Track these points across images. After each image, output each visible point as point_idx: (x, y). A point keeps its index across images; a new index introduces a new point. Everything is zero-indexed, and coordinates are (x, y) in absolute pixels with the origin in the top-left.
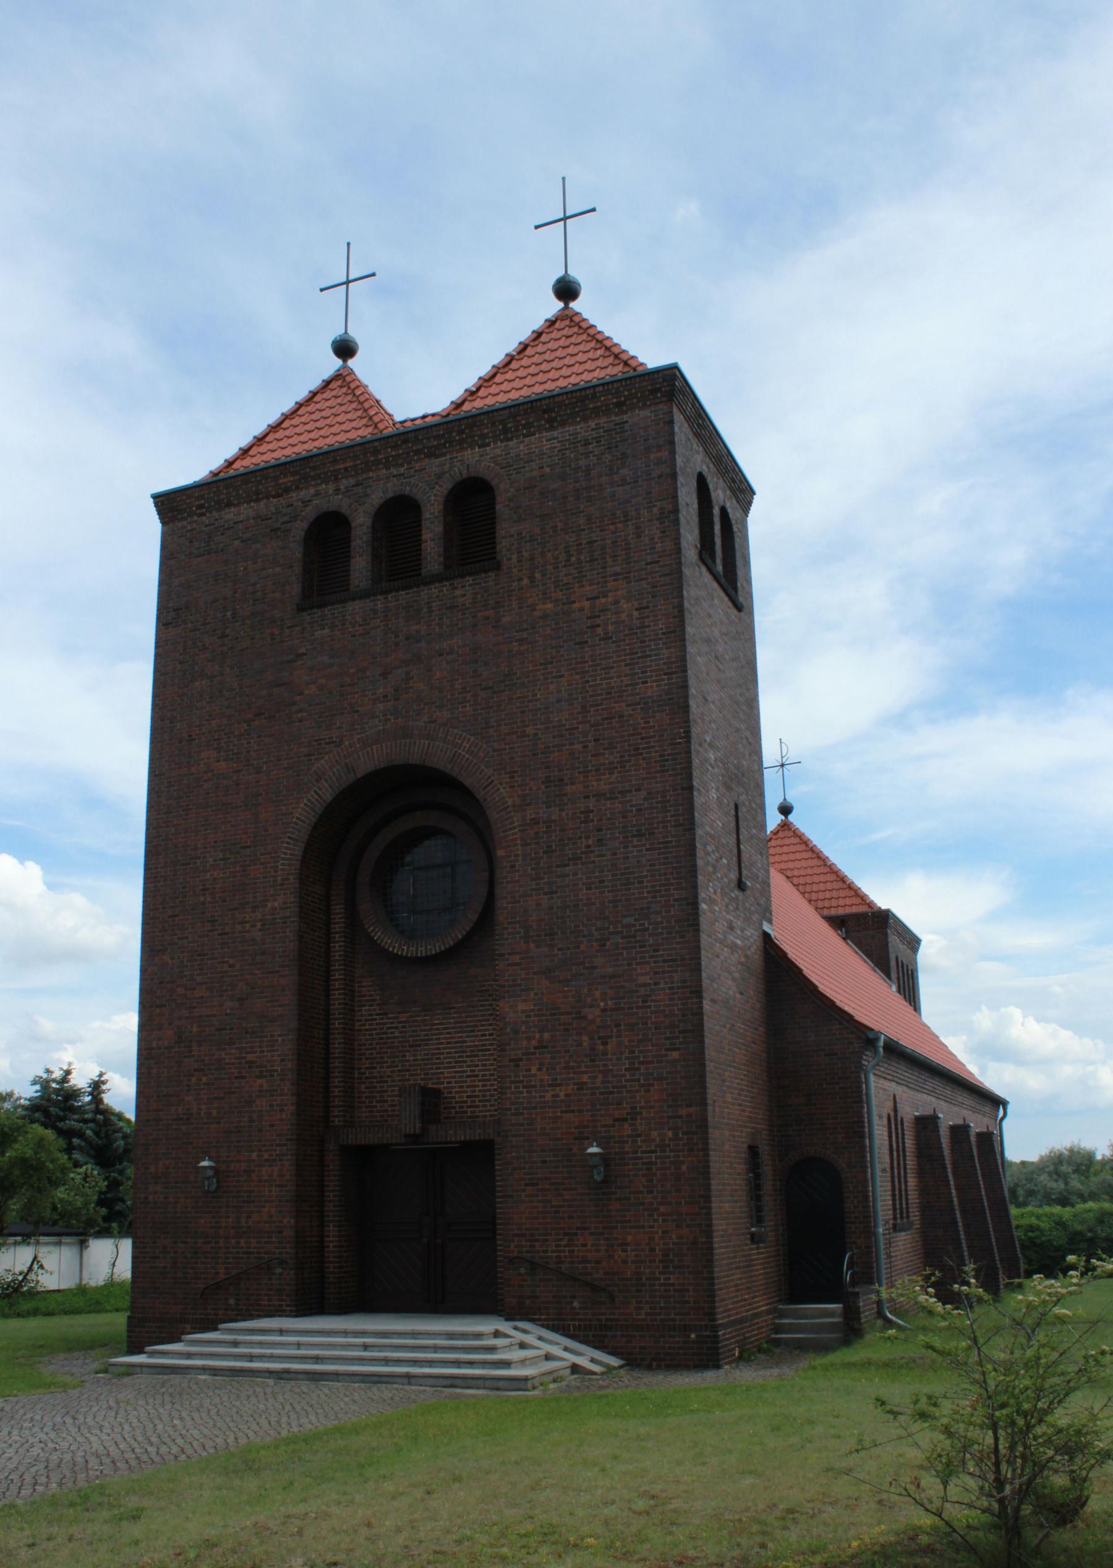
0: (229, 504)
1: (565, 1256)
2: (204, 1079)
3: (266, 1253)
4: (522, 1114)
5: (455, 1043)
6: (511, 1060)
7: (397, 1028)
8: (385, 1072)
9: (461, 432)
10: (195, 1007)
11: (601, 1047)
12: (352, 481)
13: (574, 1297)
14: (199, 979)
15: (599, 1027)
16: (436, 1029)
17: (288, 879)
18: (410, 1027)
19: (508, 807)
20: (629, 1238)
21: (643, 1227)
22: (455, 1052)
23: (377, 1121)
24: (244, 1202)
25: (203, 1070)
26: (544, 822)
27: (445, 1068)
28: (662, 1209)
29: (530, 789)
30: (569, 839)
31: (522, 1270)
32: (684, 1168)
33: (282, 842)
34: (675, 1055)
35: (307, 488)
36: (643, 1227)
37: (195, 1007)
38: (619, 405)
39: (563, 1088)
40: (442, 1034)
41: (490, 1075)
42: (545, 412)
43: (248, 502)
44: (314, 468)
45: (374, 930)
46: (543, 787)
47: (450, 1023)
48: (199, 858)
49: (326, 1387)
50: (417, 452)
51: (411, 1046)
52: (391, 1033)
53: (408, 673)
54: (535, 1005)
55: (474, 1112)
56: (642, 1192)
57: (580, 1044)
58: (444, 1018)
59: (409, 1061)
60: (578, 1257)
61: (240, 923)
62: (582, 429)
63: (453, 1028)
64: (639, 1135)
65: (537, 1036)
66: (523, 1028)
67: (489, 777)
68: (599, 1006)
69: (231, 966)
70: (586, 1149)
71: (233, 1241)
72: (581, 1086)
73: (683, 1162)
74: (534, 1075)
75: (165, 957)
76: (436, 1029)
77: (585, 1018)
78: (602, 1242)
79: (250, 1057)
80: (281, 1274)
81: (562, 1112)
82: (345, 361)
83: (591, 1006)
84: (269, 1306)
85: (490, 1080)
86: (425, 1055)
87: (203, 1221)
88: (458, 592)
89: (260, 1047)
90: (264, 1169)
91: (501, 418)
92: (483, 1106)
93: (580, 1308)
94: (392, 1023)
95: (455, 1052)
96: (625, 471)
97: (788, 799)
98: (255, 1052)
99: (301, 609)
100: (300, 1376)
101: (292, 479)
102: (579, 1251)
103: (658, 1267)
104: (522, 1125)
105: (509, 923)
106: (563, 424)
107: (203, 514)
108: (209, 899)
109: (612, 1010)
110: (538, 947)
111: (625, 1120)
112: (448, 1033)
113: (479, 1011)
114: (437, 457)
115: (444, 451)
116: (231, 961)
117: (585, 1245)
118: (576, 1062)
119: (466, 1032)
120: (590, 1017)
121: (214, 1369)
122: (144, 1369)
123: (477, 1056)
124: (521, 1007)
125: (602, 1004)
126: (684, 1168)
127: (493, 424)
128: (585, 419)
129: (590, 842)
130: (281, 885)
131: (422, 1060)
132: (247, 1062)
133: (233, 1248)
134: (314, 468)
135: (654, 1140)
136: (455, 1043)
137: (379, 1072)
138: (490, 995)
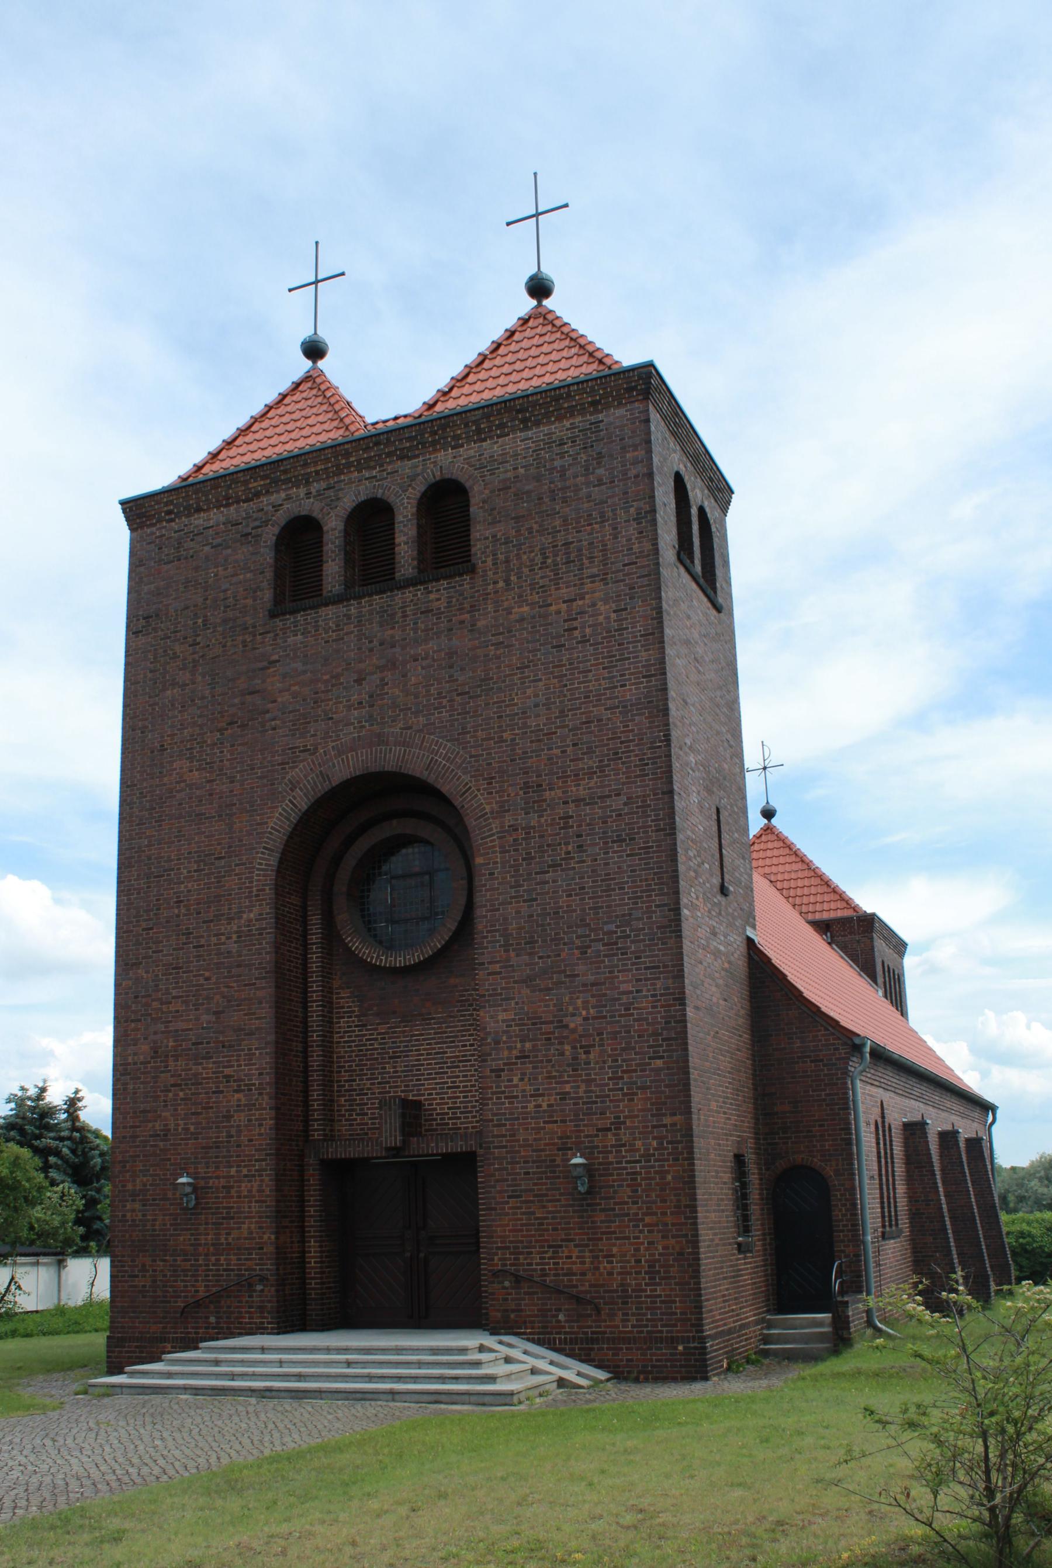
0: (199, 510)
1: (550, 1269)
2: (181, 1094)
3: (246, 1270)
4: (505, 1125)
7: (376, 1039)
8: (364, 1084)
9: (436, 433)
10: (170, 1022)
11: (584, 1056)
14: (174, 993)
17: (264, 890)
20: (615, 1250)
21: (628, 1238)
23: (358, 1135)
24: (223, 1218)
25: (180, 1085)
27: (425, 1079)
28: (648, 1219)
29: (508, 795)
30: (548, 845)
31: (507, 1284)
32: (669, 1177)
33: (257, 853)
34: (659, 1063)
35: (278, 492)
36: (628, 1238)
37: (170, 1022)
38: (594, 403)
39: (546, 1098)
42: (518, 411)
44: (285, 472)
46: (521, 792)
47: (430, 1034)
49: (308, 1405)
51: (390, 1058)
53: (382, 679)
54: (515, 1015)
56: (627, 1203)
57: (562, 1054)
58: (423, 1029)
60: (563, 1269)
61: (215, 935)
62: (558, 429)
64: (624, 1145)
65: (519, 1045)
66: (504, 1038)
67: (467, 784)
69: (207, 979)
70: (570, 1160)
71: (213, 1258)
73: (668, 1172)
74: (516, 1086)
75: (139, 971)
77: (566, 1026)
78: (587, 1254)
79: (227, 1071)
80: (262, 1291)
81: (544, 1122)
82: (315, 362)
83: (573, 1015)
84: (250, 1323)
85: (471, 1091)
86: (405, 1066)
87: (182, 1238)
88: (432, 596)
89: (238, 1061)
91: (474, 418)
92: (465, 1118)
93: (566, 1321)
95: (436, 1064)
97: (771, 803)
98: (233, 1066)
99: (273, 615)
100: (283, 1394)
102: (563, 1263)
103: (644, 1279)
104: (504, 1136)
105: (488, 932)
106: (537, 424)
107: (172, 520)
108: (183, 911)
109: (595, 1018)
110: (517, 955)
111: (609, 1129)
113: (459, 1021)
114: (409, 458)
115: (417, 452)
116: (207, 974)
117: (570, 1257)
118: (557, 1071)
119: (445, 1043)
120: (572, 1025)
121: (196, 1389)
123: (458, 1067)
124: (502, 1016)
125: (584, 1013)
126: (669, 1177)
127: (466, 425)
128: (560, 419)
129: (570, 848)
131: (403, 1071)
132: (225, 1077)
133: (213, 1265)
134: (285, 472)
135: (638, 1150)
137: (359, 1085)
138: (471, 1005)
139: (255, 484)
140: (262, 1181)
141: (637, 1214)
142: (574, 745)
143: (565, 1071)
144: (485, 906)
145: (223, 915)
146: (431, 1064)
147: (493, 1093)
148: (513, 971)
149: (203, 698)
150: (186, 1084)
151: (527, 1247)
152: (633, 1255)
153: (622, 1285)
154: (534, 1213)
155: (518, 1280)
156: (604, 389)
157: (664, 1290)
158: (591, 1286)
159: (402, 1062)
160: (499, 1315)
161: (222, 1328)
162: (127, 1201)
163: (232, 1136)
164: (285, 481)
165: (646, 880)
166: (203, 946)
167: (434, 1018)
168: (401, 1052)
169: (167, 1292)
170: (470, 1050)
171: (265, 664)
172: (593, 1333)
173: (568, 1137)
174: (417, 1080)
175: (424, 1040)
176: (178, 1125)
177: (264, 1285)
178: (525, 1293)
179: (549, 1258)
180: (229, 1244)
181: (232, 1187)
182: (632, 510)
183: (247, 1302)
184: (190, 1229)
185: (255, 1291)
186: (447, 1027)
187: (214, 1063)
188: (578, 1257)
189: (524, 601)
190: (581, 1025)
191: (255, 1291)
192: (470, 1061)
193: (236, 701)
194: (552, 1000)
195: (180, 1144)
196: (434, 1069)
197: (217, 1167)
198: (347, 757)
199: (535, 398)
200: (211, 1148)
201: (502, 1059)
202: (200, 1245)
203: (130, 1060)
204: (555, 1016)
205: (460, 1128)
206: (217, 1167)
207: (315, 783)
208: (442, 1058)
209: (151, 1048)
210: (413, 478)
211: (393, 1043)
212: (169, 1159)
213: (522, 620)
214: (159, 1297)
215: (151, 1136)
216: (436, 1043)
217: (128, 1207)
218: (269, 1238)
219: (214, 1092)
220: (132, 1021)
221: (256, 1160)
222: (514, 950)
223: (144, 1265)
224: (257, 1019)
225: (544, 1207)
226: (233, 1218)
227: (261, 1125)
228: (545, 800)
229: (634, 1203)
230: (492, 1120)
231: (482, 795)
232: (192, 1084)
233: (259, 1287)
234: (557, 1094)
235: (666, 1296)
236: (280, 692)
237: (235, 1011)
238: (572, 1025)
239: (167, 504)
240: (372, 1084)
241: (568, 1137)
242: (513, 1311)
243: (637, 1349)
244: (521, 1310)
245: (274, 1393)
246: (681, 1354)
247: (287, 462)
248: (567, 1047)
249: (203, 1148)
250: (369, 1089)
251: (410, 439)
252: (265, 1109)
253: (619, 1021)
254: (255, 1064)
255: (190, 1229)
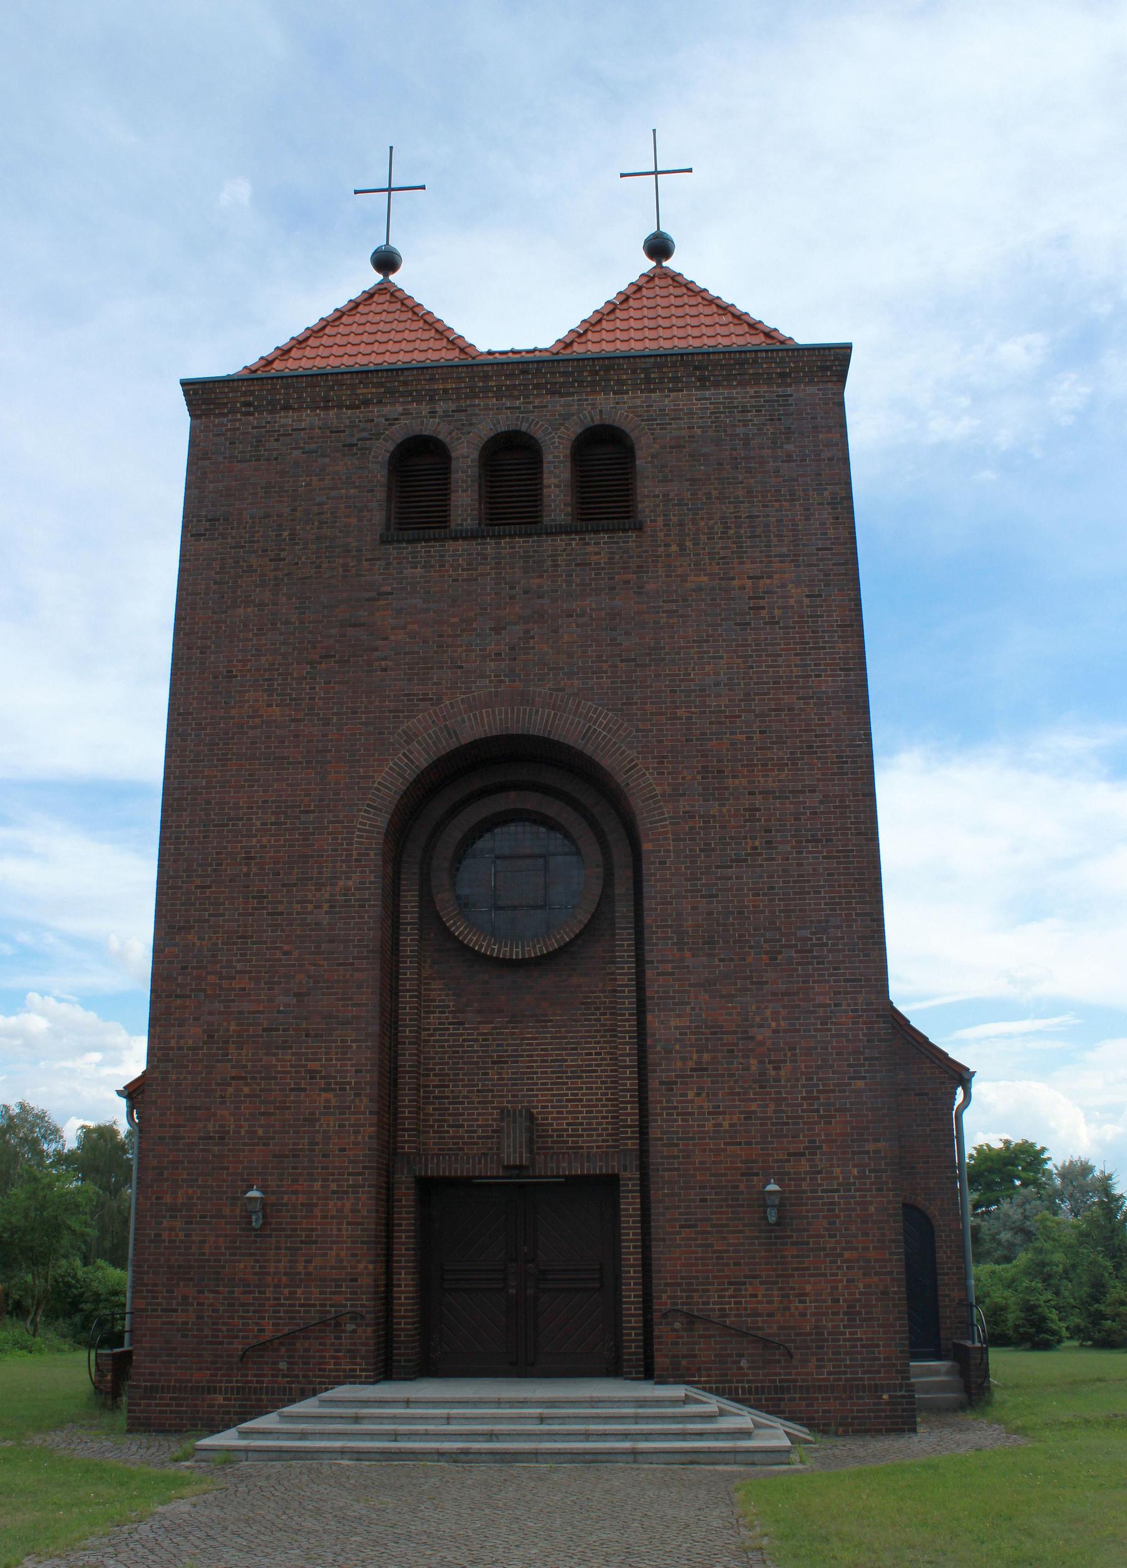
0: (287, 407)
1: (730, 1309)
2: (246, 1090)
5: (552, 1061)
6: (661, 1083)
8: (460, 1091)
9: (596, 373)
10: (234, 1001)
11: (773, 1073)
12: (452, 406)
13: (742, 1355)
14: (239, 966)
15: (769, 1050)
16: (528, 1045)
18: (494, 1040)
19: (656, 795)
20: (808, 1288)
22: (552, 1072)
23: (449, 1149)
24: (302, 1242)
25: (245, 1078)
26: (701, 816)
27: (538, 1090)
28: (847, 1254)
29: (683, 778)
30: (731, 838)
31: (677, 1325)
32: (872, 1209)
33: (360, 810)
34: (860, 1084)
35: (393, 404)
37: (234, 1001)
38: (782, 375)
40: (536, 1050)
41: (597, 1100)
42: (696, 368)
43: (313, 409)
44: (405, 383)
45: (454, 924)
47: (546, 1038)
48: (241, 819)
50: (537, 386)
52: (469, 1046)
53: (527, 632)
54: (691, 1021)
55: (577, 1142)
57: (747, 1068)
59: (493, 1079)
60: (746, 1309)
62: (742, 395)
63: (551, 1044)
64: (820, 1172)
66: (677, 1047)
67: (632, 760)
68: (769, 1026)
69: (285, 953)
72: (749, 1116)
74: (692, 1101)
75: (190, 937)
76: (528, 1045)
78: (776, 1292)
80: (354, 1331)
82: (386, 275)
83: (761, 1026)
84: (337, 1370)
85: (597, 1106)
86: (513, 1073)
87: (242, 1265)
88: (591, 549)
89: (327, 1054)
90: (331, 1203)
91: (644, 366)
93: (749, 1368)
94: (468, 1034)
95: (552, 1072)
96: (789, 447)
99: (639, 528)
100: (483, 1457)
101: (374, 390)
103: (842, 1320)
104: (675, 1157)
106: (717, 385)
107: (249, 414)
109: (785, 1031)
111: (803, 1154)
112: (542, 1050)
114: (562, 395)
115: (571, 390)
116: (286, 947)
118: (741, 1087)
119: (566, 1049)
120: (759, 1037)
122: (250, 1454)
125: (774, 1024)
126: (872, 1209)
127: (634, 372)
128: (743, 384)
129: (757, 843)
130: (357, 860)
134: (405, 383)
136: (552, 1061)
138: (598, 1009)
139: (365, 391)
140: (357, 1199)
141: (835, 1249)
142: (761, 732)
143: (750, 1087)
144: (655, 898)
145: (311, 879)
146: (546, 1073)
147: (663, 1108)
148: (689, 973)
149: (287, 622)
150: (253, 1078)
151: (703, 1284)
152: (831, 1294)
153: (816, 1327)
154: (711, 1245)
155: (691, 1320)
156: (795, 362)
157: (866, 1333)
158: (780, 1328)
159: (509, 1068)
160: (667, 1361)
161: (297, 1376)
162: (164, 1217)
163: (317, 1144)
164: (402, 394)
165: (846, 886)
166: (282, 914)
167: (551, 1021)
168: (508, 1056)
169: (220, 1330)
170: (596, 1060)
171: (373, 594)
172: (781, 1381)
173: (753, 1162)
174: (528, 1090)
175: (537, 1044)
176: (241, 1126)
177: (358, 1325)
178: (700, 1336)
179: (730, 1297)
180: (308, 1274)
181: (316, 1205)
182: (826, 493)
183: (333, 1344)
184: (254, 1255)
185: (344, 1331)
186: (567, 1032)
187: (293, 1054)
188: (764, 1296)
189: (701, 570)
190: (769, 1038)
191: (344, 1331)
192: (596, 1071)
193: (333, 631)
194: (735, 1008)
195: (244, 1151)
196: (552, 1078)
197: (295, 1180)
198: (481, 713)
199: (717, 357)
200: (287, 1156)
201: (675, 1070)
202: (268, 1274)
203: (173, 1043)
204: (738, 1026)
205: (582, 1148)
206: (295, 1180)
207: (437, 736)
208: (561, 1066)
209: (204, 1031)
210: (566, 417)
211: (498, 1045)
212: (227, 1168)
213: (699, 590)
214: (207, 1336)
215: (200, 1138)
216: (553, 1049)
217: (165, 1224)
218: (366, 1268)
219: (292, 1090)
220: (177, 996)
221: (349, 1174)
222: (690, 950)
223: (185, 1298)
224: (353, 1005)
225: (725, 1238)
226: (316, 1242)
227: (356, 1132)
228: (727, 788)
229: (831, 1236)
230: (661, 1139)
231: (651, 774)
232: (262, 1078)
233: (350, 1327)
234: (741, 1113)
235: (867, 1339)
236: (393, 629)
237: (323, 994)
238: (759, 1037)
239: (245, 394)
240: (469, 1092)
241: (753, 1162)
242: (684, 1356)
243: (836, 1398)
244: (695, 1356)
245: (470, 1457)
246: (887, 1403)
247: (409, 373)
248: (753, 1061)
249: (275, 1156)
250: (464, 1097)
251: (565, 374)
252: (364, 1113)
253: (815, 1037)
254: (350, 1059)
255: (254, 1255)
